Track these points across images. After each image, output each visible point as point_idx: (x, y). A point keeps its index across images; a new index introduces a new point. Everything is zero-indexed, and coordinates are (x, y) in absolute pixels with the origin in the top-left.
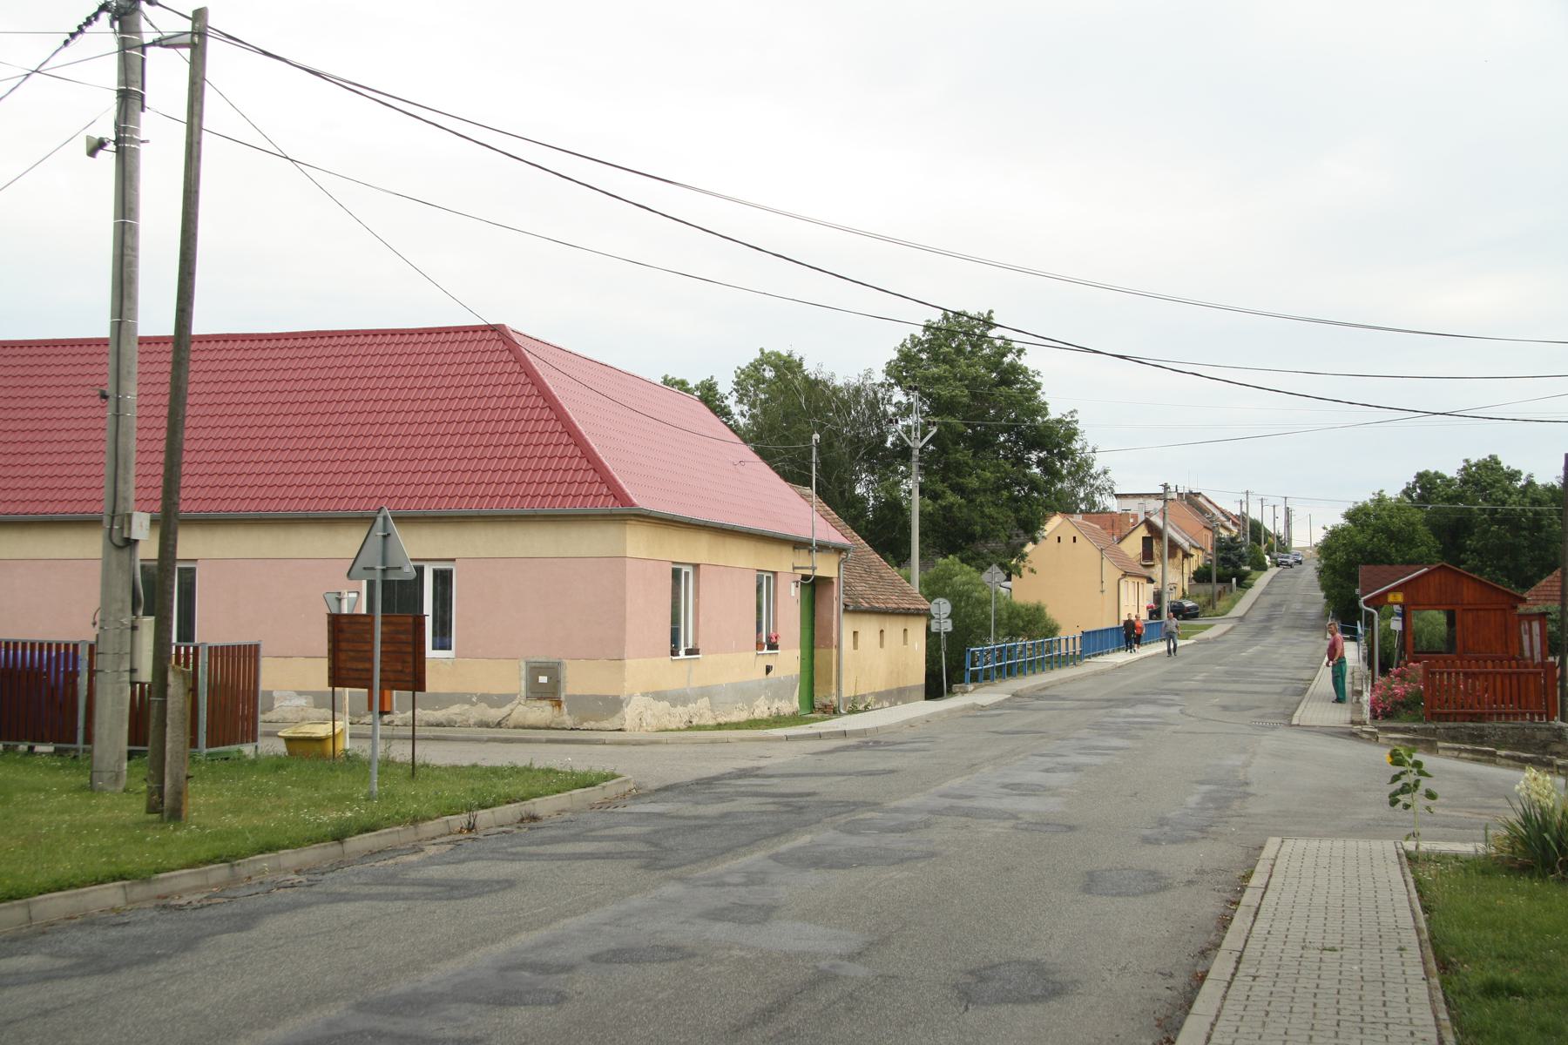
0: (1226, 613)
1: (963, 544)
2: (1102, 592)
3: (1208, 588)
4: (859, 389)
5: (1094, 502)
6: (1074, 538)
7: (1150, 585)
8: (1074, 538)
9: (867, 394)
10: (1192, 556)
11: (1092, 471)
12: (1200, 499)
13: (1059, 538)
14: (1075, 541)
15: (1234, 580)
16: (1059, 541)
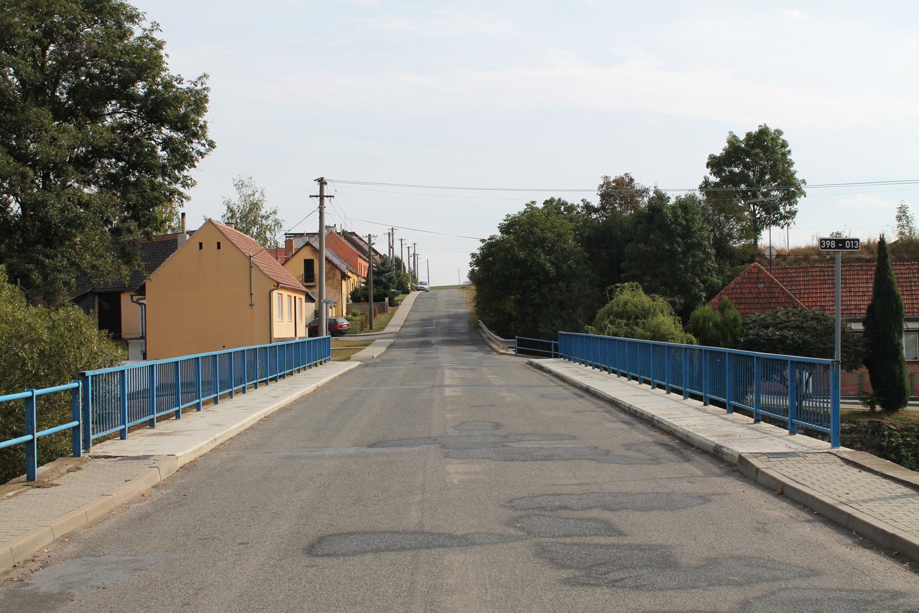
0: (383, 329)
1: (110, 226)
2: (251, 305)
3: (365, 306)
4: (546, 239)
5: (266, 238)
6: (219, 244)
7: (310, 304)
8: (219, 244)
9: (69, 152)
10: (349, 277)
11: (263, 212)
12: (354, 237)
13: (201, 244)
14: (219, 247)
15: (387, 299)
16: (201, 247)
